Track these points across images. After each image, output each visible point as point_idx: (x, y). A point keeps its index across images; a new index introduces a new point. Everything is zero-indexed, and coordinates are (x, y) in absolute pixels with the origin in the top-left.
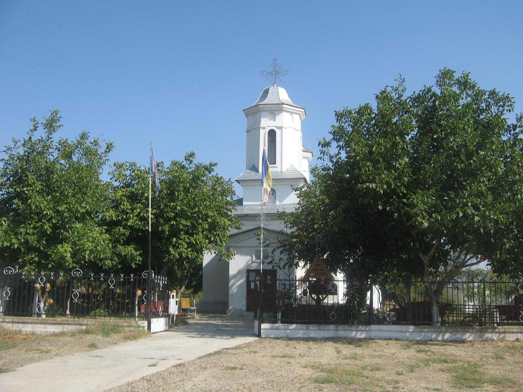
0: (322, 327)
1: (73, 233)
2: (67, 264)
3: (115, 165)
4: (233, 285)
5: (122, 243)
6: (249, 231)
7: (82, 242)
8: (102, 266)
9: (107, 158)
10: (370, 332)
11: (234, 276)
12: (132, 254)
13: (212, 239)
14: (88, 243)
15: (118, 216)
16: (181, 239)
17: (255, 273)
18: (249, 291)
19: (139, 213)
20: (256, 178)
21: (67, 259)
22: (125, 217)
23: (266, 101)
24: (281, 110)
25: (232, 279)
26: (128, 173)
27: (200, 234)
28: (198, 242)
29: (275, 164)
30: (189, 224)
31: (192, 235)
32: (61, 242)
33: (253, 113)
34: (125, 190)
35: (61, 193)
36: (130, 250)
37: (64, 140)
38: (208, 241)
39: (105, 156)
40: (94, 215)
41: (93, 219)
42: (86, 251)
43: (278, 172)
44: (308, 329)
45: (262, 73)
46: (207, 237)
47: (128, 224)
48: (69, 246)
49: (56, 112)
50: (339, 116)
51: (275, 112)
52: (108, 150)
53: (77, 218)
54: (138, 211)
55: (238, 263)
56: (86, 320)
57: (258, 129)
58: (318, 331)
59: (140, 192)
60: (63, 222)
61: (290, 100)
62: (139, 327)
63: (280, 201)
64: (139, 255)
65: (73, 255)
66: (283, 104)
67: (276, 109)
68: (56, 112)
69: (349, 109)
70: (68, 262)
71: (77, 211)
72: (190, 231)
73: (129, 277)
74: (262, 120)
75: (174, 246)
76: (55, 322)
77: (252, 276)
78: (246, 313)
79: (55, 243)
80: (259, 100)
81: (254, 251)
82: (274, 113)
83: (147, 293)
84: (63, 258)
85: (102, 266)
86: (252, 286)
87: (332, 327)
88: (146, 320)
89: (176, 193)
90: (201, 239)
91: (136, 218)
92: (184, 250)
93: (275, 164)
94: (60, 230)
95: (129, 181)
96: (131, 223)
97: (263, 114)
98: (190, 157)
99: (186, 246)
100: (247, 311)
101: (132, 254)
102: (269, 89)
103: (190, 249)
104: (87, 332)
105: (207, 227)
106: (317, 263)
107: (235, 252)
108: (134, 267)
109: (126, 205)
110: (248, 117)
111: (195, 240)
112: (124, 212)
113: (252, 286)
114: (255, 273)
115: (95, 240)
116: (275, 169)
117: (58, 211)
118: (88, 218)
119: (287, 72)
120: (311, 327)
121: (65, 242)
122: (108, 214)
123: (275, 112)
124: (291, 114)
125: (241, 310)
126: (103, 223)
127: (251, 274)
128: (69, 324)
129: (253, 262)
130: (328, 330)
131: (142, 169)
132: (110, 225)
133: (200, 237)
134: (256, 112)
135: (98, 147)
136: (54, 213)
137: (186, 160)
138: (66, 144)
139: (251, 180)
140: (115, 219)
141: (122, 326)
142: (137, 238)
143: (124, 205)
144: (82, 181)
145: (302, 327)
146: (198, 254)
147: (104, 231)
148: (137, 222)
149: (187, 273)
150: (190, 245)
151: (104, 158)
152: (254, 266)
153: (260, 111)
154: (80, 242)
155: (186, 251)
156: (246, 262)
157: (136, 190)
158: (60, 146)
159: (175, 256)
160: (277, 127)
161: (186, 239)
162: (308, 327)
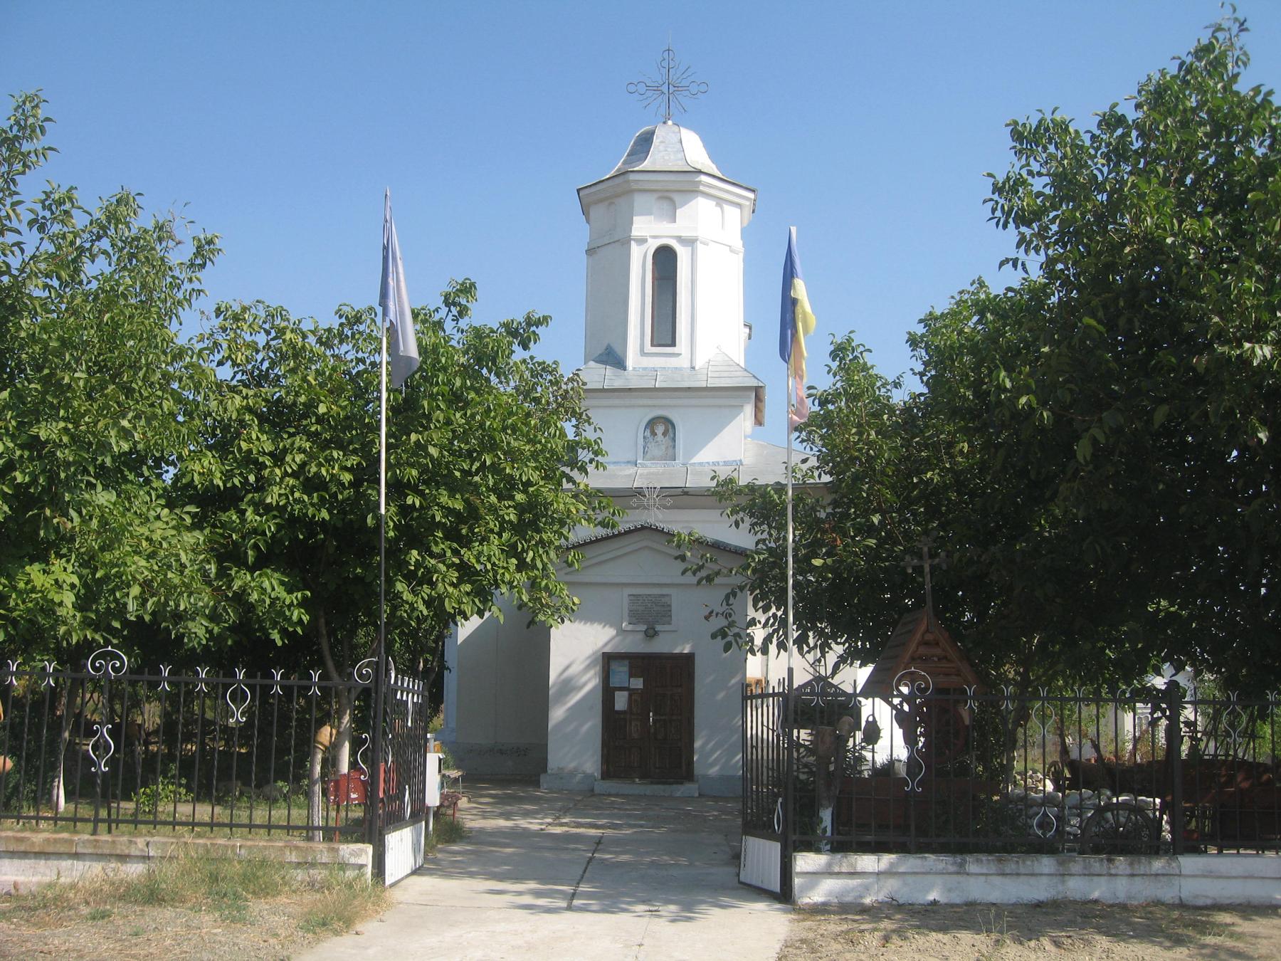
0: (1012, 863)
1: (85, 521)
2: (62, 629)
3: (218, 312)
5: (251, 560)
6: (592, 542)
7: (117, 553)
8: (180, 637)
9: (196, 285)
10: (1176, 881)
12: (274, 601)
14: (136, 558)
15: (228, 476)
16: (432, 555)
17: (626, 662)
19: (303, 465)
20: (618, 384)
21: (61, 612)
22: (252, 478)
23: (646, 165)
24: (692, 191)
26: (261, 339)
27: (494, 539)
30: (459, 506)
31: (466, 542)
32: (41, 555)
33: (608, 200)
34: (251, 393)
35: (45, 381)
36: (269, 587)
37: (63, 190)
38: (514, 561)
39: (190, 280)
40: (149, 468)
41: (147, 481)
42: (129, 586)
44: (961, 871)
45: (632, 88)
46: (511, 551)
47: (269, 500)
48: (70, 569)
49: (33, 101)
50: (1027, 139)
51: (676, 197)
52: (199, 261)
53: (102, 472)
54: (298, 460)
55: (576, 647)
56: (141, 842)
57: (625, 242)
58: (997, 880)
59: (303, 399)
60: (52, 478)
61: (714, 166)
62: (343, 866)
64: (300, 605)
65: (83, 604)
66: (700, 172)
67: (678, 187)
68: (33, 101)
69: (1058, 117)
70: (65, 623)
71: (104, 447)
72: (461, 529)
73: (324, 683)
75: (410, 577)
76: (22, 848)
77: (620, 674)
78: (602, 786)
79: (21, 558)
80: (624, 163)
81: (626, 601)
82: (671, 200)
83: (373, 740)
84: (48, 608)
85: (180, 637)
86: (621, 701)
87: (1046, 864)
88: (370, 842)
89: (425, 403)
91: (291, 481)
92: (450, 589)
93: (673, 344)
94: (43, 508)
95: (266, 365)
96: (276, 497)
97: (639, 200)
98: (459, 296)
100: (603, 778)
101: (274, 601)
102: (653, 133)
104: (151, 895)
105: (513, 517)
106: (929, 637)
107: (576, 600)
108: (279, 643)
109: (258, 441)
110: (596, 212)
112: (249, 461)
113: (621, 701)
114: (626, 662)
115: (159, 552)
116: (673, 359)
117: (34, 444)
118: (131, 477)
119: (703, 88)
120: (974, 865)
121: (59, 556)
122: (197, 467)
123: (676, 197)
124: (718, 204)
126: (177, 496)
128: (76, 856)
130: (1032, 875)
131: (306, 326)
132: (209, 503)
133: (493, 547)
135: (171, 244)
136: (22, 447)
137: (447, 303)
138: (68, 206)
139: (603, 390)
140: (218, 482)
141: (282, 865)
142: (295, 550)
143: (249, 440)
144: (120, 342)
145: (941, 866)
147: (188, 520)
148: (297, 495)
151: (187, 286)
152: (636, 644)
154: (107, 557)
155: (456, 592)
157: (288, 394)
158: (48, 214)
159: (413, 609)
160: (680, 239)
161: (449, 553)
162: (962, 865)
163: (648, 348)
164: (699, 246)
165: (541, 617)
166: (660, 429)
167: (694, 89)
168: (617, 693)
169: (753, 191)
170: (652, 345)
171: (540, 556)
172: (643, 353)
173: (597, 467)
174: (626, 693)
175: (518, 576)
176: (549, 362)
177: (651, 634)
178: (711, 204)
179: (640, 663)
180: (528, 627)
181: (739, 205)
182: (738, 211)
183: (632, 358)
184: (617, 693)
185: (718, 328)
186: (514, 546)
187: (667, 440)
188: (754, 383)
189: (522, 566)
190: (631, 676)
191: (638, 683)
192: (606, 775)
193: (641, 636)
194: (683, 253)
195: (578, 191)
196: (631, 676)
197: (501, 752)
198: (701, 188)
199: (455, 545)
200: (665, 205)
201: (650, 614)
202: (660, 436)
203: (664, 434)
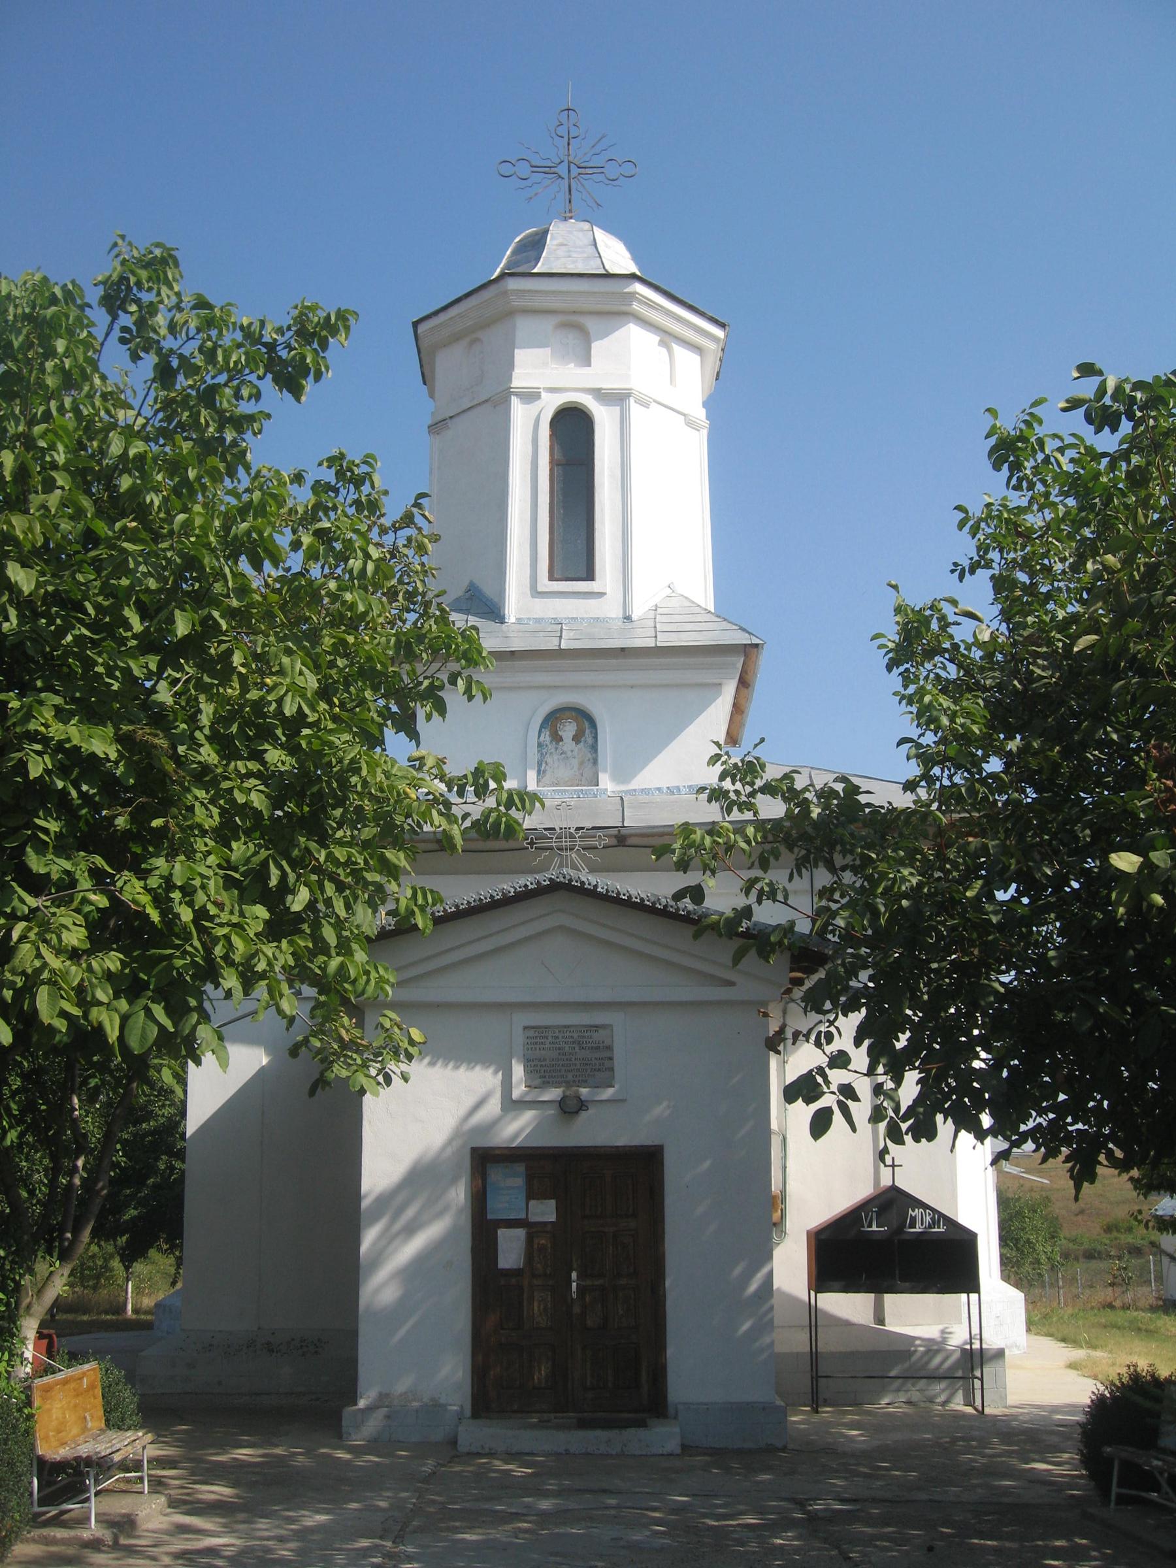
4: (377, 1260)
11: (385, 1201)
13: (299, 901)
17: (521, 1168)
18: (491, 1288)
24: (618, 313)
25: (375, 1217)
28: (186, 915)
29: (590, 576)
31: (125, 853)
38: (261, 912)
43: (605, 620)
45: (506, 169)
46: (250, 885)
51: (591, 323)
55: (421, 1114)
67: (588, 310)
74: (521, 356)
78: (474, 1434)
81: (519, 1038)
90: (212, 890)
92: (55, 963)
93: (590, 576)
97: (524, 326)
99: (75, 937)
100: (476, 1414)
102: (546, 232)
103: (112, 961)
107: (416, 1035)
111: (161, 900)
113: (511, 1250)
114: (521, 1168)
116: (592, 602)
119: (628, 169)
123: (591, 323)
124: (662, 343)
125: (435, 1408)
127: (496, 1175)
129: (511, 1105)
133: (203, 869)
134: (486, 324)
146: (177, 1011)
149: (93, 1173)
150: (115, 927)
152: (517, 1129)
153: (511, 313)
156: (469, 1101)
160: (602, 395)
161: (85, 883)
163: (545, 584)
164: (635, 409)
165: (340, 1071)
166: (568, 730)
167: (612, 171)
168: (501, 1232)
169: (722, 326)
170: (552, 578)
171: (328, 902)
172: (536, 593)
173: (468, 690)
174: (521, 1233)
175: (269, 949)
176: (355, 456)
178: (651, 339)
179: (545, 1167)
180: (312, 1092)
181: (697, 349)
182: (696, 358)
183: (517, 601)
184: (501, 1232)
185: (664, 554)
186: (261, 873)
187: (581, 750)
188: (744, 639)
189: (281, 926)
190: (531, 1195)
191: (545, 1211)
192: (494, 1393)
193: (551, 1112)
194: (604, 419)
195: (416, 325)
196: (531, 1195)
197: (270, 1348)
198: (636, 306)
199: (99, 861)
200: (572, 338)
201: (569, 1061)
202: (568, 743)
203: (577, 738)
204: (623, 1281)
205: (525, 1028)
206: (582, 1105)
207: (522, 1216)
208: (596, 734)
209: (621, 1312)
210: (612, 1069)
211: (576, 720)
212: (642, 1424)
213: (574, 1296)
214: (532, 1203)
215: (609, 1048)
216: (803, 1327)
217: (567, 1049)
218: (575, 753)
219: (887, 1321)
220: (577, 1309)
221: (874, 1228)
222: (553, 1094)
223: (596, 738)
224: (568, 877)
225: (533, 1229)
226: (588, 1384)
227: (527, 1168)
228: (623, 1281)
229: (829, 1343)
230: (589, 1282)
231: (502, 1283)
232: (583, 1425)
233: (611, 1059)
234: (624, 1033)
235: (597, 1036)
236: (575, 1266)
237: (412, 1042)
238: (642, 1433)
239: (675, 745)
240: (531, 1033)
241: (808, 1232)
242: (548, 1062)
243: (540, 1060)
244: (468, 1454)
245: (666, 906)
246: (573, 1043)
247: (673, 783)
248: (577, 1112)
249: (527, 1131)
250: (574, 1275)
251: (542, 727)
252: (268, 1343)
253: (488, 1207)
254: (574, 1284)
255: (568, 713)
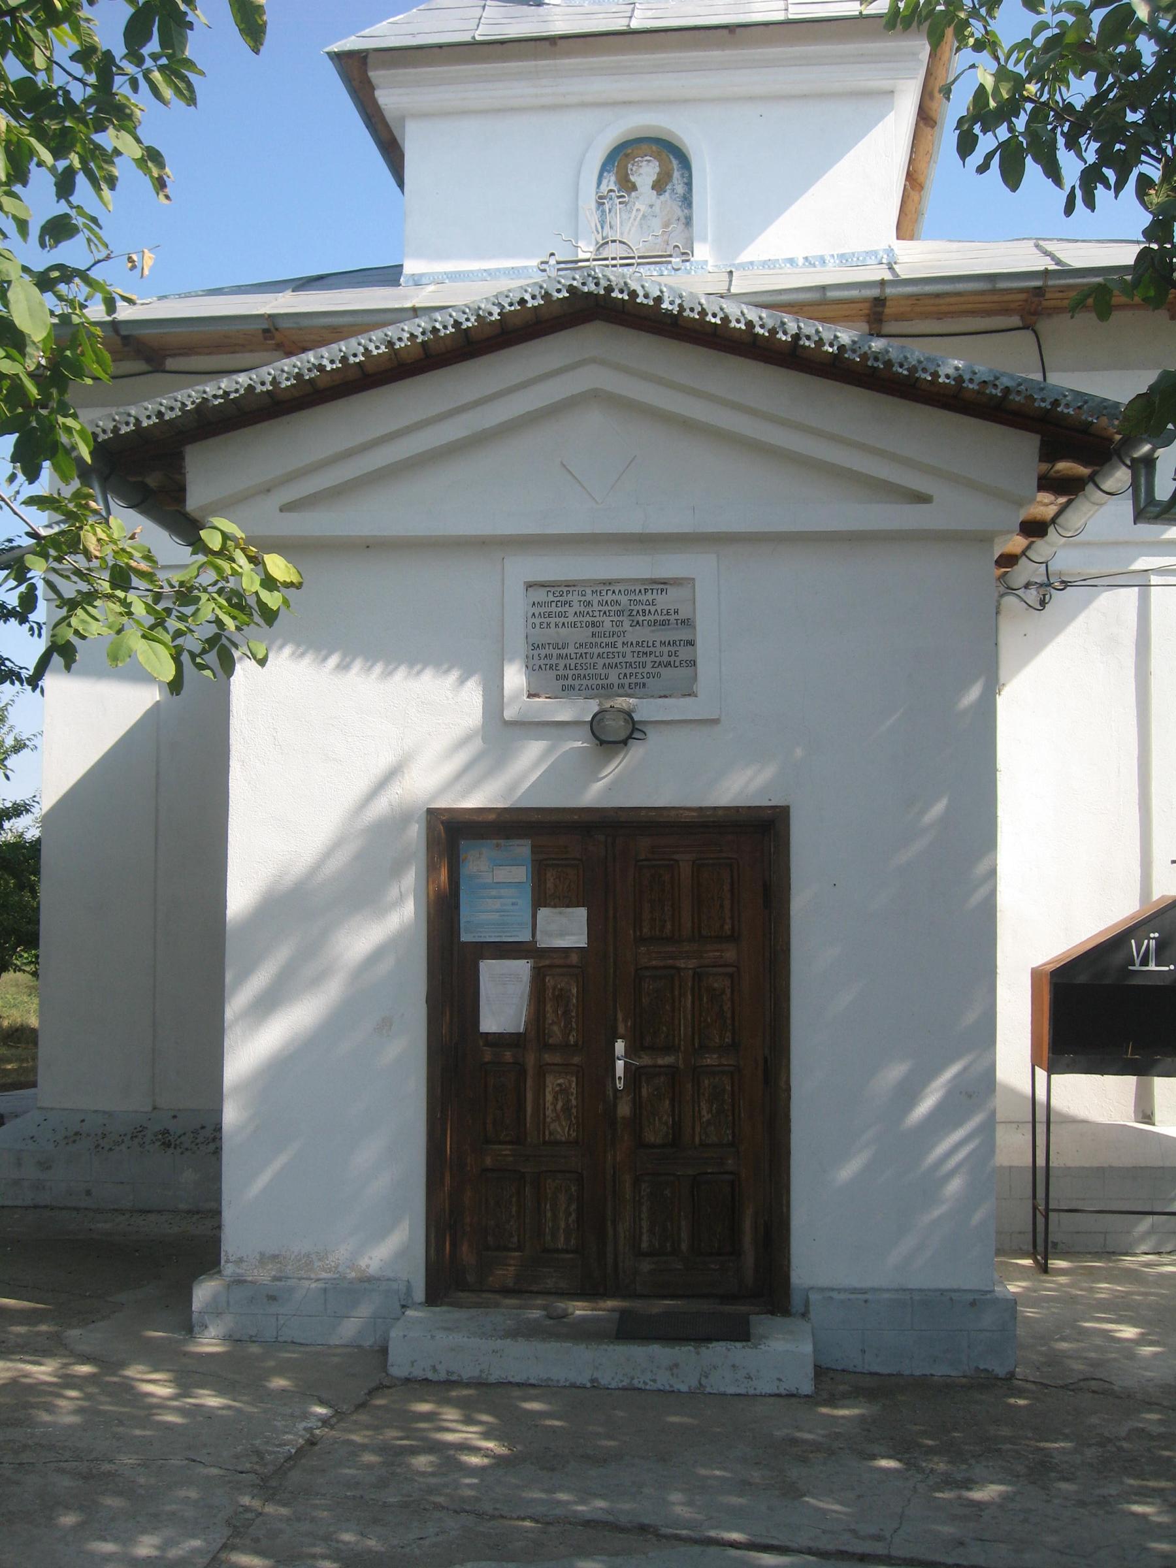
17: (523, 849)
63: (731, 242)
77: (500, 895)
78: (430, 1340)
81: (517, 605)
113: (503, 1001)
114: (523, 849)
125: (349, 1290)
152: (523, 778)
166: (645, 172)
168: (489, 969)
174: (522, 968)
177: (612, 736)
179: (568, 847)
184: (489, 969)
187: (667, 203)
190: (541, 899)
191: (567, 929)
192: (452, 1273)
193: (579, 743)
196: (541, 899)
201: (611, 650)
203: (659, 186)
204: (710, 1060)
205: (530, 586)
206: (634, 730)
207: (525, 937)
208: (690, 176)
209: (706, 1117)
210: (693, 663)
211: (658, 156)
212: (740, 1333)
213: (620, 1085)
214: (543, 913)
215: (687, 623)
216: (1018, 1124)
217: (607, 624)
218: (657, 209)
219: (1158, 1117)
220: (624, 1109)
221: (1152, 967)
222: (582, 709)
223: (689, 185)
224: (604, 283)
225: (548, 966)
226: (644, 1245)
227: (535, 849)
228: (710, 1060)
229: (1066, 1154)
230: (646, 1060)
231: (488, 1057)
232: (628, 1330)
233: (691, 643)
234: (715, 596)
235: (664, 601)
236: (621, 1029)
237: (269, 583)
238: (737, 1352)
239: (818, 189)
240: (541, 595)
241: (1036, 974)
242: (571, 650)
243: (556, 646)
244: (408, 1380)
245: (797, 337)
246: (620, 613)
247: (812, 252)
248: (625, 742)
249: (533, 777)
250: (620, 1047)
251: (604, 169)
252: (166, 1132)
253: (463, 920)
254: (620, 1064)
255: (644, 147)
